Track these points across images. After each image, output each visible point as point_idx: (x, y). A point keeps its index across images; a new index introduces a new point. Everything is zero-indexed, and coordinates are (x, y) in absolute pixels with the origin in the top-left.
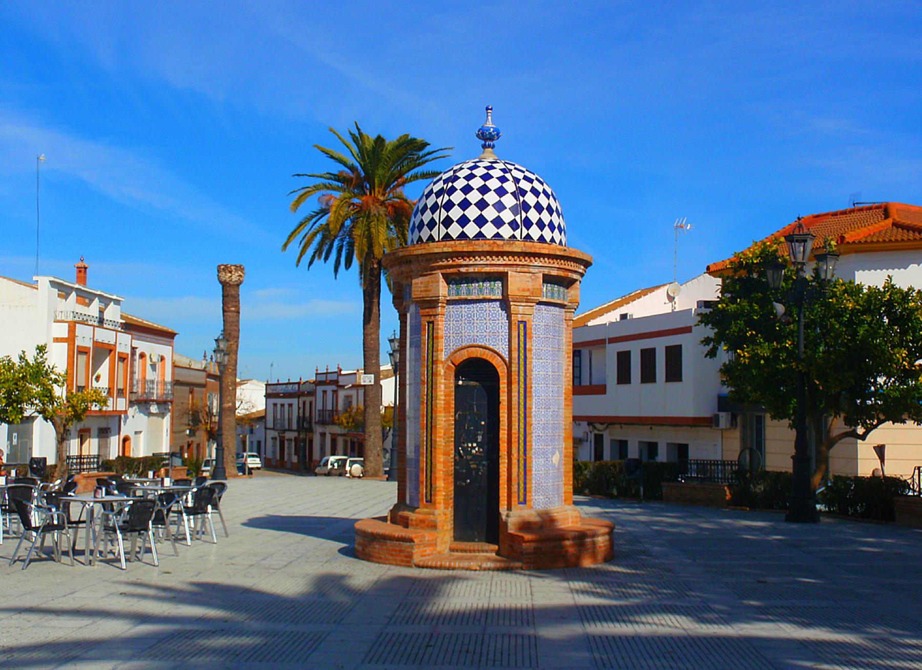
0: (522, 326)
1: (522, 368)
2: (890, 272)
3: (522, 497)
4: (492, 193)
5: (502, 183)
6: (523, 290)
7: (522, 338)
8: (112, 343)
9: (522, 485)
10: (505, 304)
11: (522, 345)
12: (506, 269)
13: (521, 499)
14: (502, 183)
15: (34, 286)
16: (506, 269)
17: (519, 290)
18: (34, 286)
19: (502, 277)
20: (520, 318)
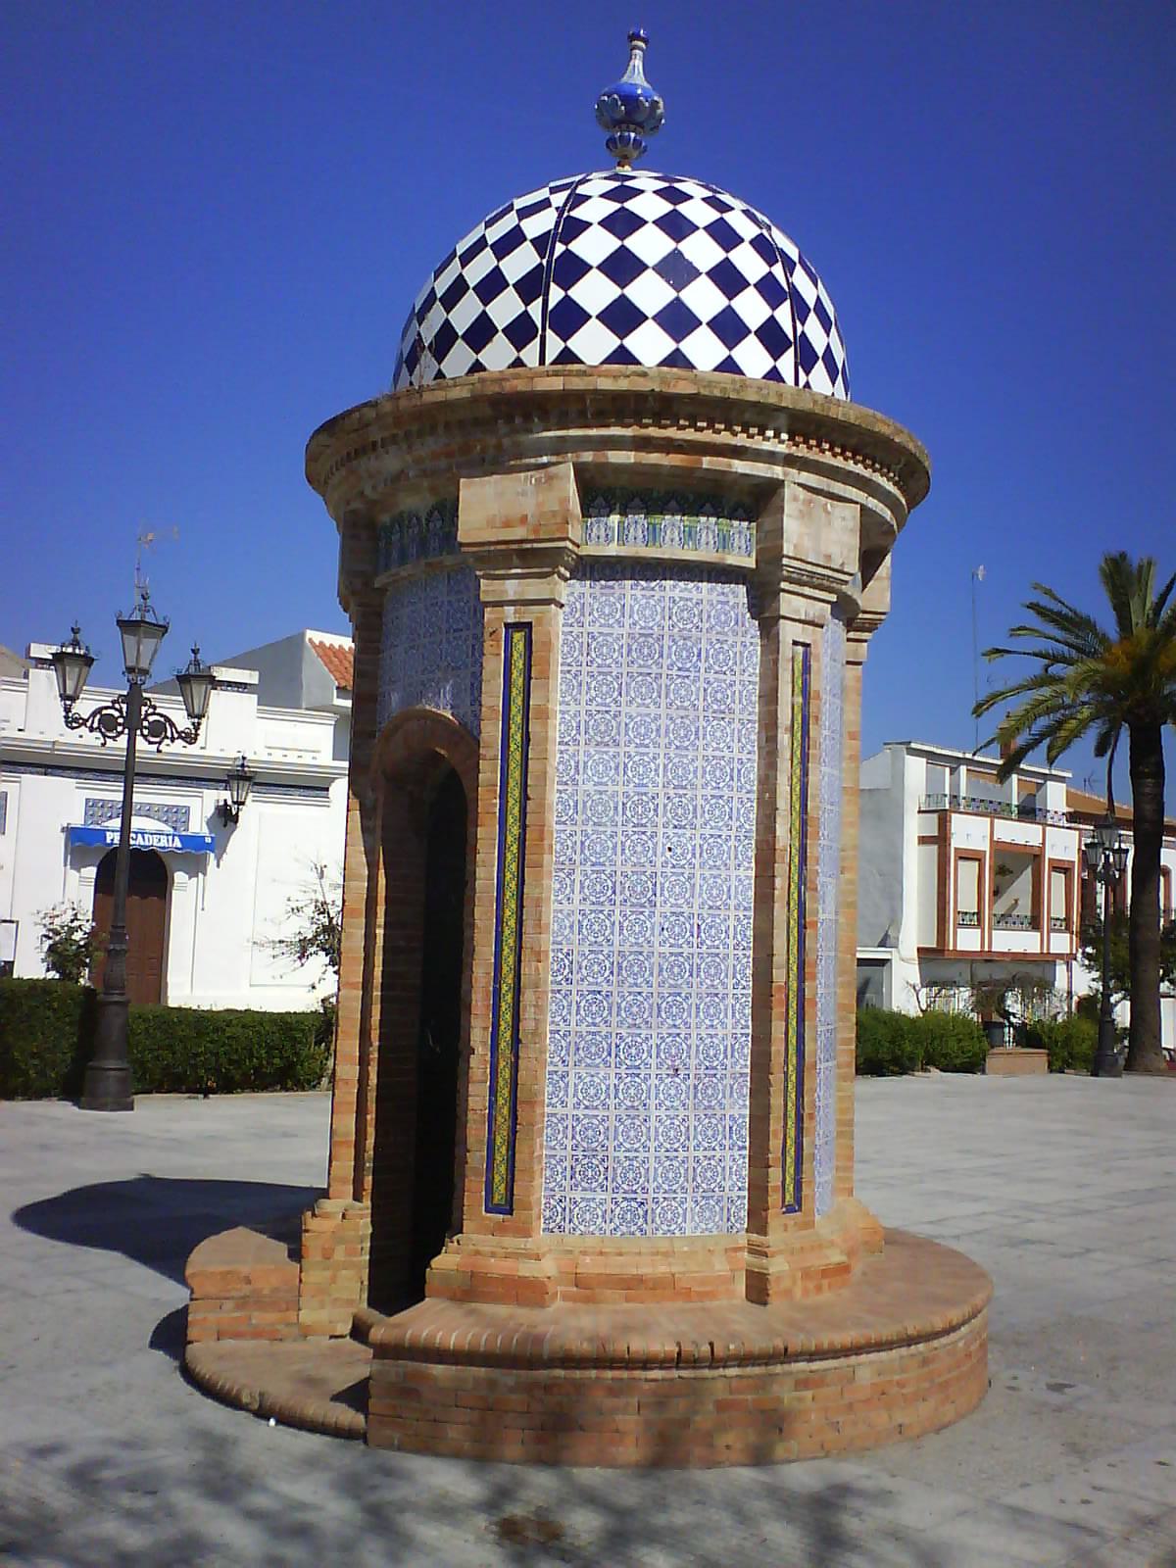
0: (518, 637)
1: (515, 774)
2: (340, 789)
3: (500, 1189)
4: (649, 276)
5: (622, 236)
6: (507, 524)
7: (518, 679)
8: (125, 636)
9: (502, 1151)
10: (762, 589)
11: (518, 701)
12: (778, 472)
13: (499, 1197)
14: (622, 236)
15: (1172, 694)
16: (778, 472)
17: (491, 523)
18: (1172, 694)
19: (757, 502)
20: (510, 614)
